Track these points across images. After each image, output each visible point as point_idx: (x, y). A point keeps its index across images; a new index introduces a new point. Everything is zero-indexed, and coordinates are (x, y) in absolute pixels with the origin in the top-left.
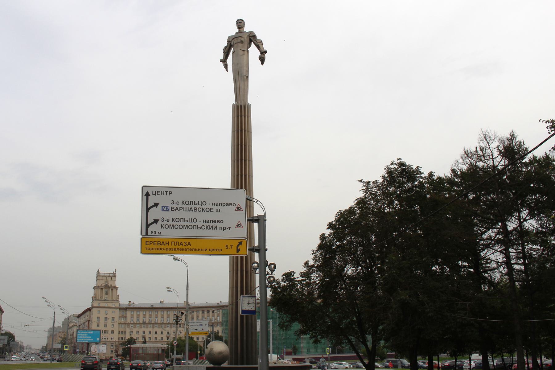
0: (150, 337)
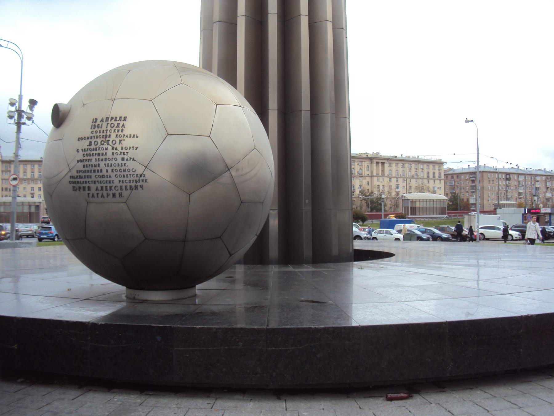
0: (40, 195)
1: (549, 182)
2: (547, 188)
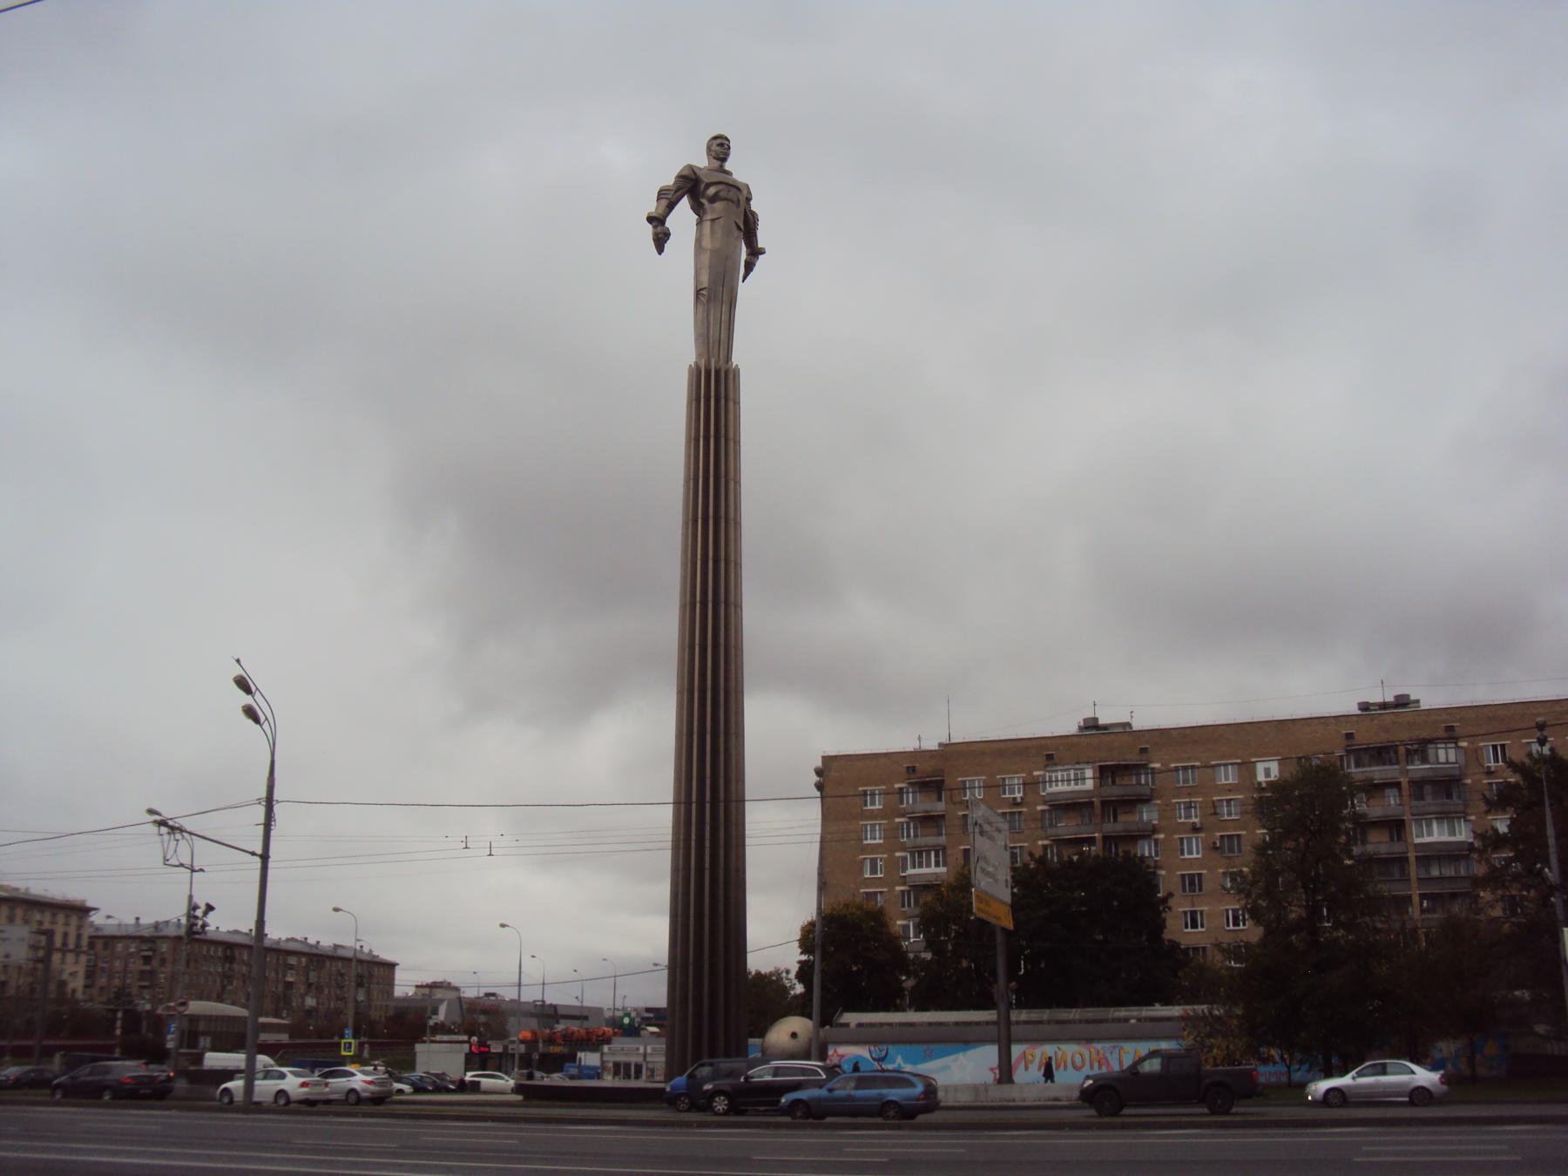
1: (314, 970)
2: (310, 985)
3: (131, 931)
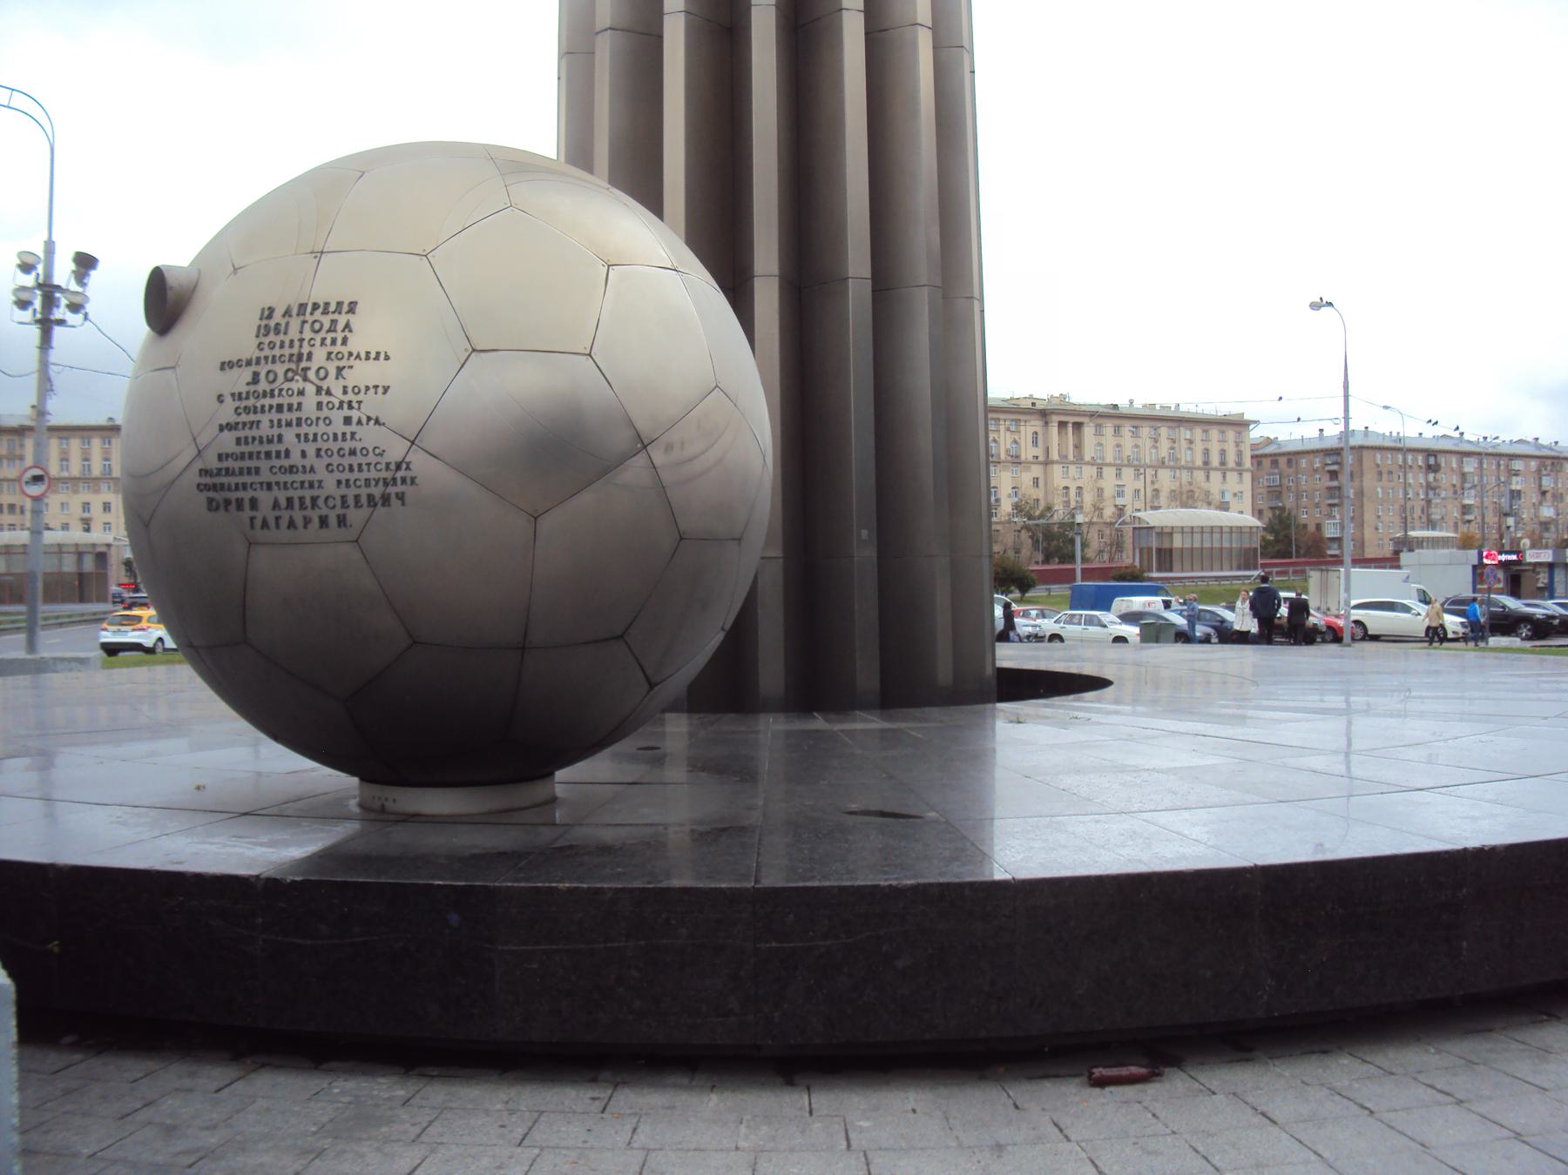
0: (109, 523)
2: (1544, 493)
3: (1317, 446)
